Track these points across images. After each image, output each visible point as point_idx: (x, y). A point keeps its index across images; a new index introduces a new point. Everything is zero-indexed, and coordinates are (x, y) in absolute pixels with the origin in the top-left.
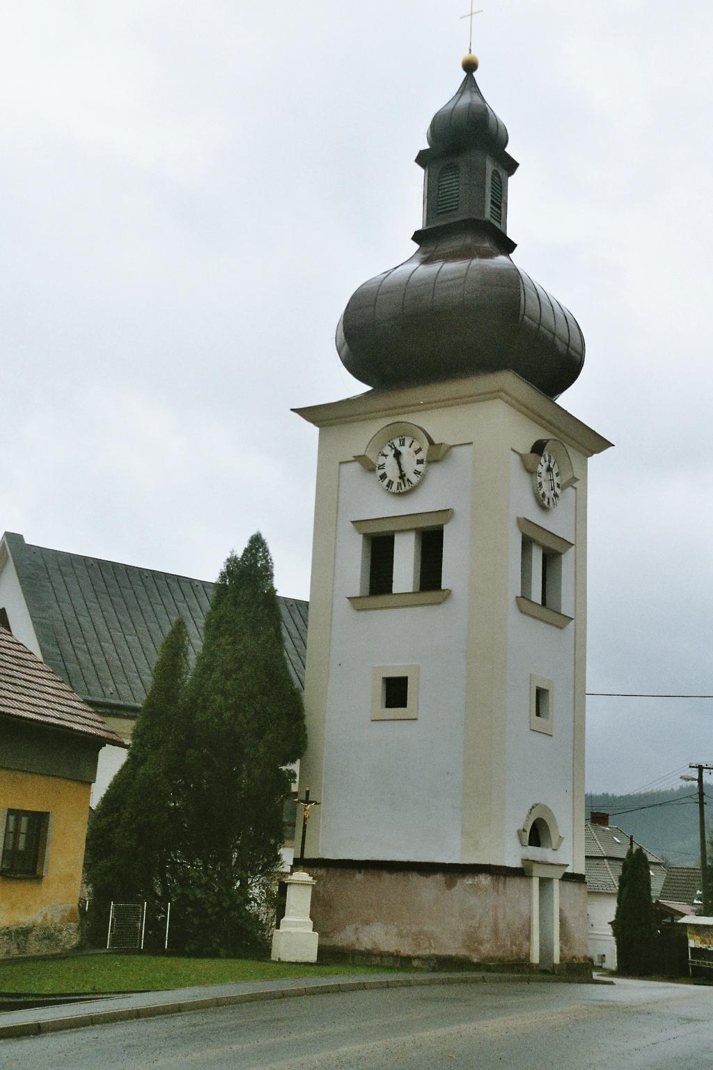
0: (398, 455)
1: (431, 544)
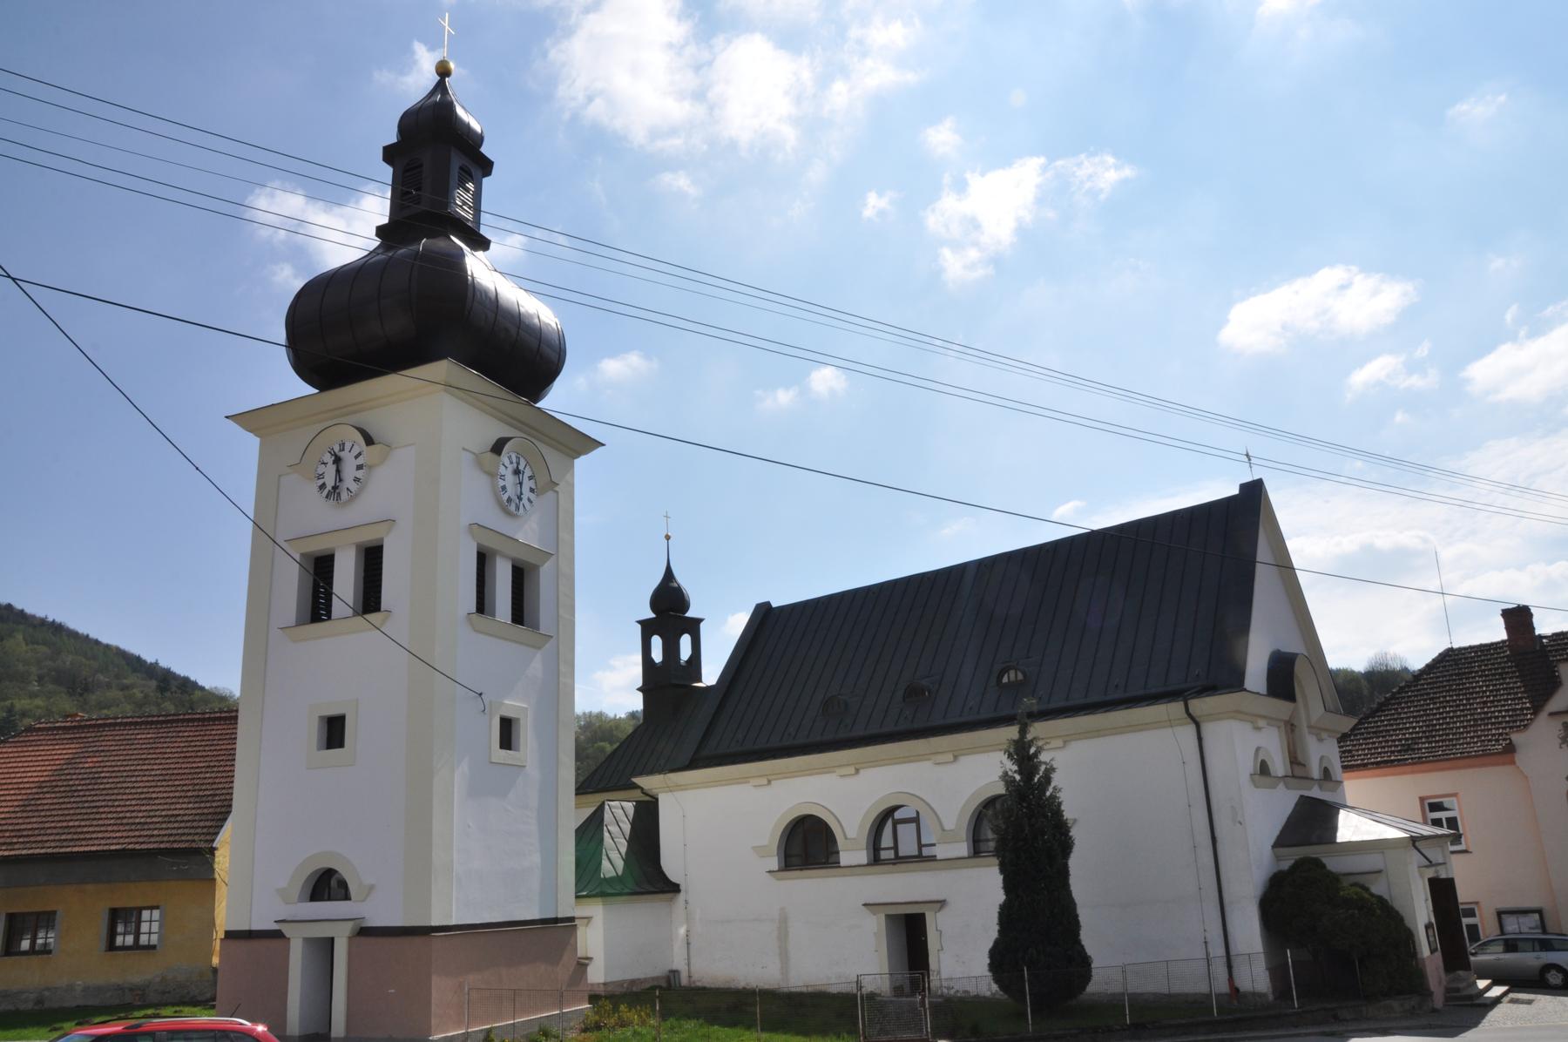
1: (372, 558)
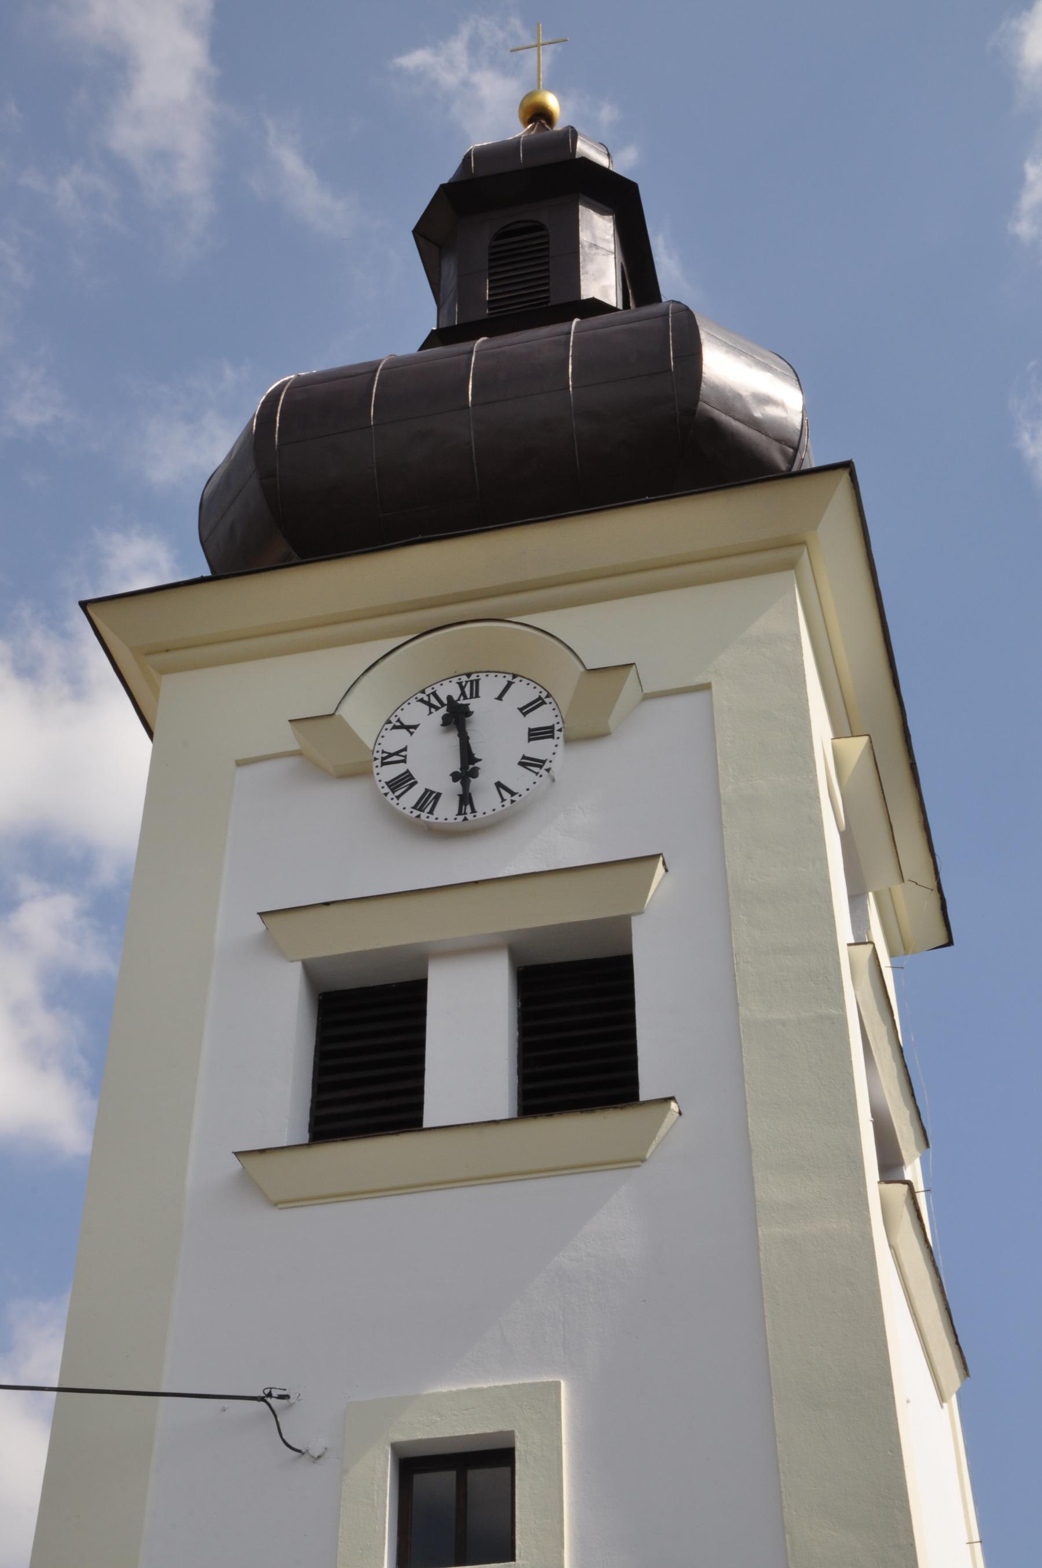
0: (457, 717)
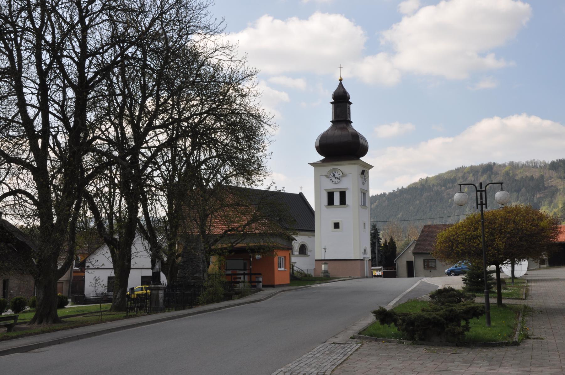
1: (343, 195)
